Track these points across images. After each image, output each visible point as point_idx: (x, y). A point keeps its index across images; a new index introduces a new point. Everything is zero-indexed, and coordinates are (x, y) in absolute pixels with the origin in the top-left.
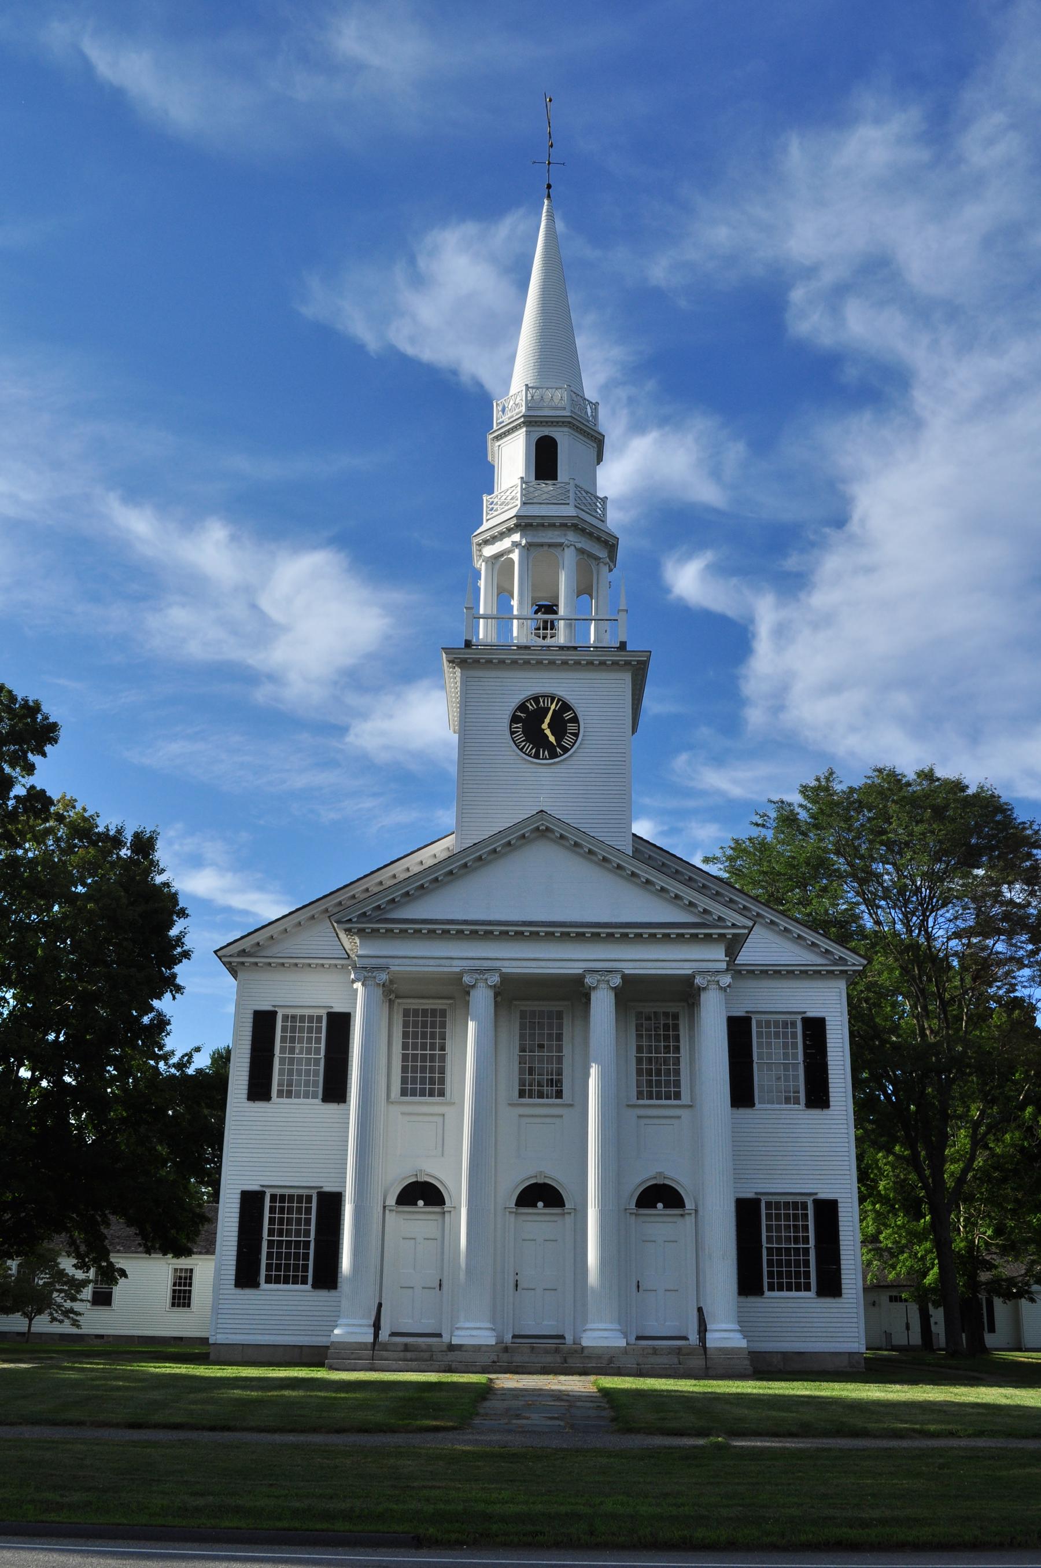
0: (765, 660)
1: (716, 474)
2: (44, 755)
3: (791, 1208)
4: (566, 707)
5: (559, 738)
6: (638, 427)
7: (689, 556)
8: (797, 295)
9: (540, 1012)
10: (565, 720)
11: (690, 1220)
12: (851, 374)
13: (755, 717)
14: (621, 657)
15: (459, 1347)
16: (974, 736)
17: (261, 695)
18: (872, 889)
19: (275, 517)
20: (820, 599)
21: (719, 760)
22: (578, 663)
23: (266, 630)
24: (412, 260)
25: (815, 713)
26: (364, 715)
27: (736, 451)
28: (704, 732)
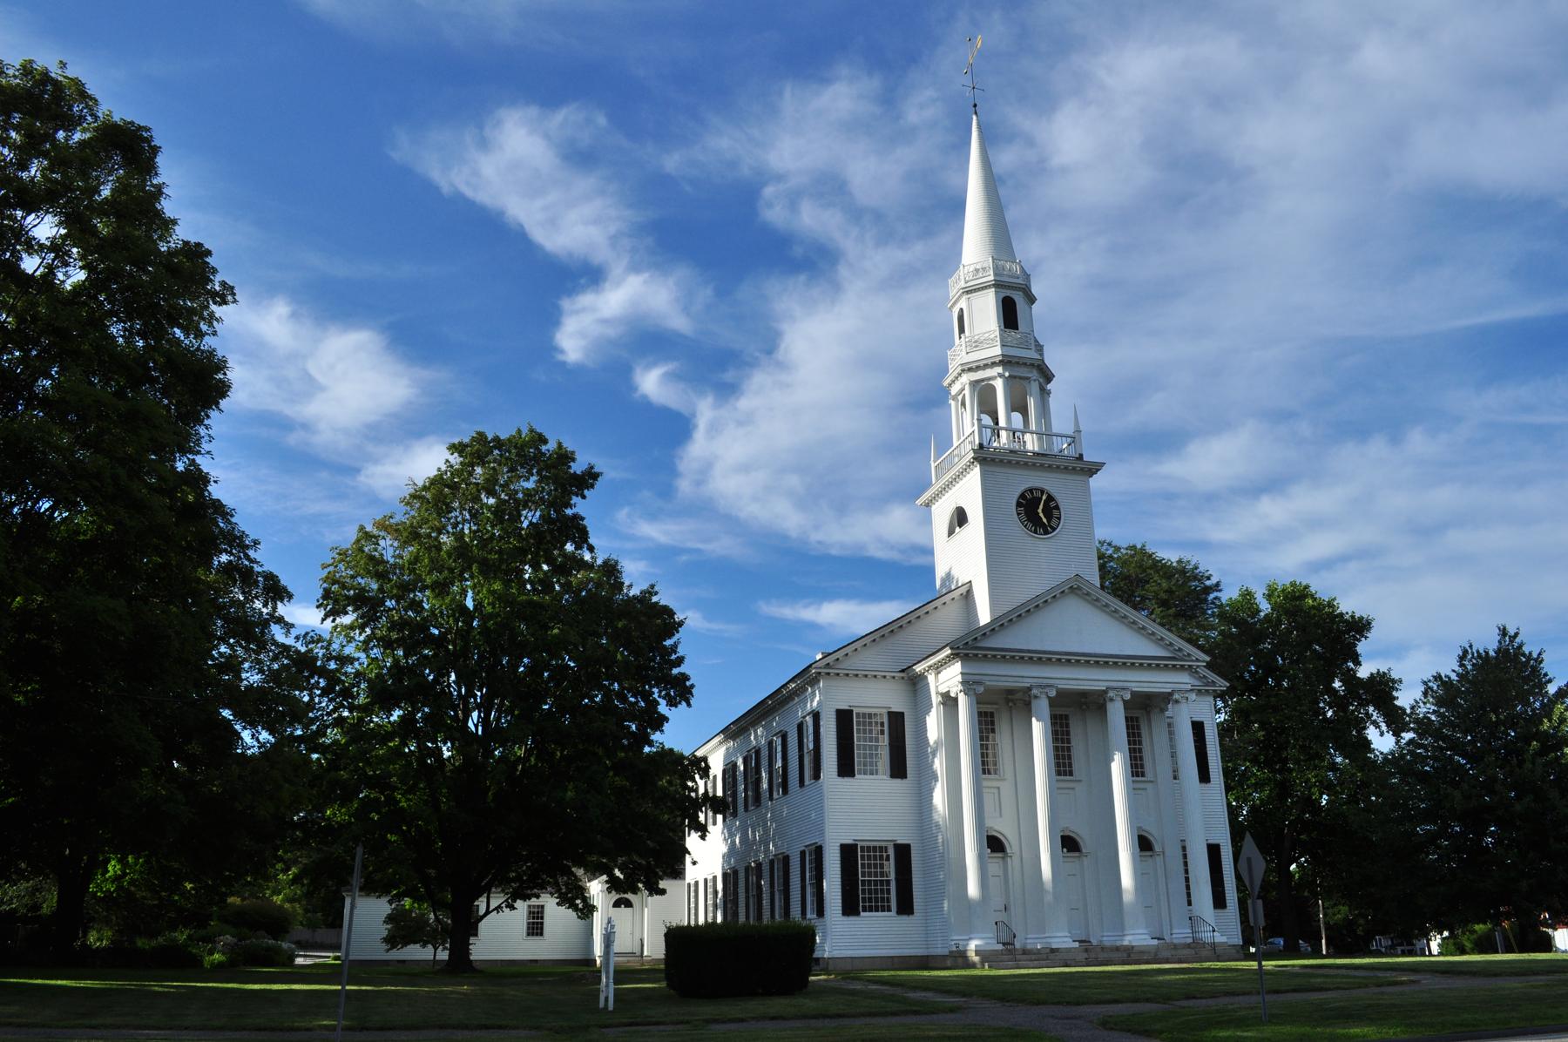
0: (699, 447)
1: (686, 310)
2: (584, 497)
3: (877, 851)
4: (1050, 498)
5: (1049, 518)
6: (635, 268)
7: (654, 364)
8: (769, 191)
9: (1074, 713)
10: (1052, 508)
11: (1159, 859)
12: (798, 251)
13: (684, 486)
14: (1079, 465)
15: (1057, 950)
16: (842, 508)
17: (293, 439)
18: (1214, 634)
19: (333, 303)
20: (744, 403)
21: (653, 516)
22: (1050, 466)
23: (311, 387)
24: (481, 127)
25: (729, 486)
26: (376, 461)
27: (706, 294)
28: (646, 494)
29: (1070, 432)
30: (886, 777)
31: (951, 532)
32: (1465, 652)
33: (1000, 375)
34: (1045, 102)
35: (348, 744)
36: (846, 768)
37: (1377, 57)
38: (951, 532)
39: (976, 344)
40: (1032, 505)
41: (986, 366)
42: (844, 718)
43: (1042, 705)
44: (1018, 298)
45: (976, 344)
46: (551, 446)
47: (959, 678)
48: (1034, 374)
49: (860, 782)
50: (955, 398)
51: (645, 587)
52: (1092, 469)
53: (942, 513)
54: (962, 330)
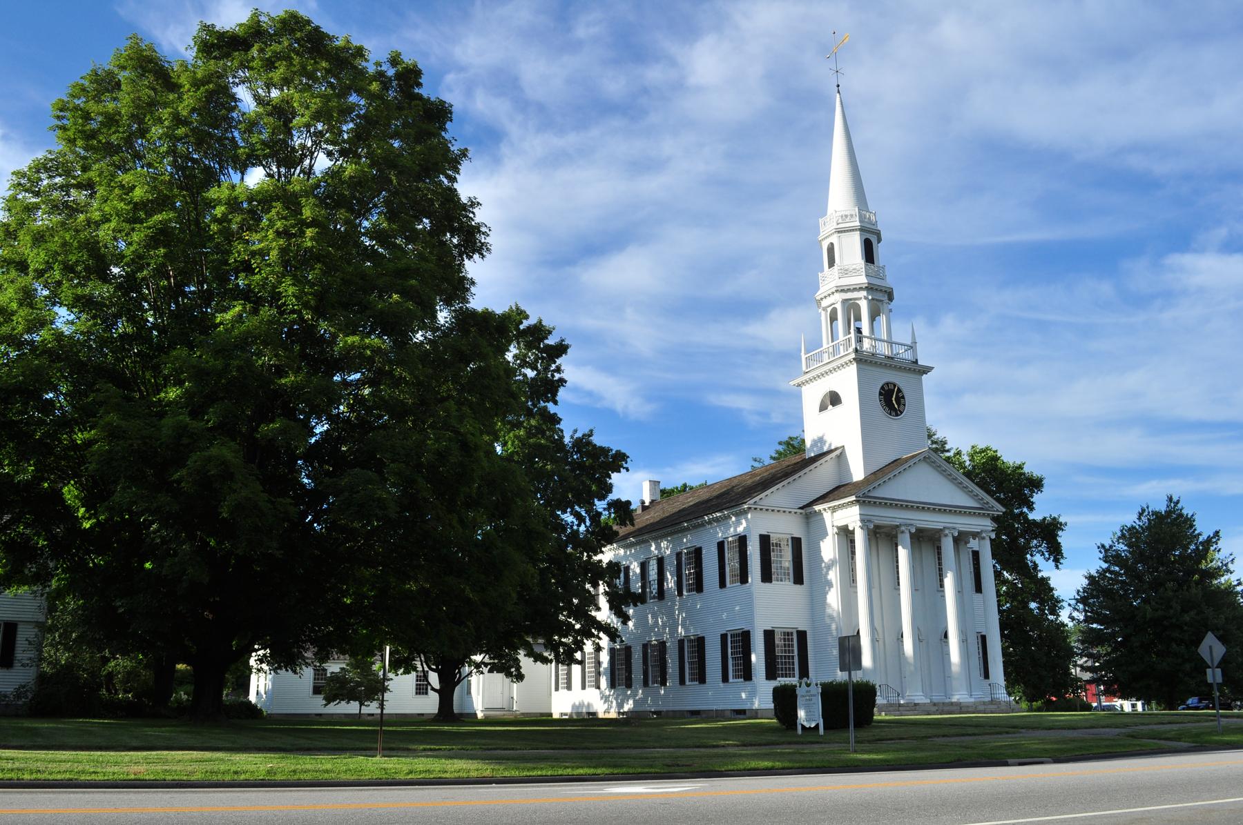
4: (899, 390)
8: (450, 78)
14: (913, 367)
29: (909, 342)
30: (791, 583)
31: (823, 408)
32: (1143, 510)
33: (866, 298)
34: (689, 31)
35: (589, 557)
36: (767, 577)
37: (951, 31)
38: (823, 408)
39: (845, 272)
40: (890, 397)
41: (855, 290)
42: (765, 540)
43: (906, 538)
44: (874, 239)
45: (845, 272)
46: (532, 321)
47: (858, 517)
48: (885, 298)
49: (775, 586)
50: (825, 309)
51: (587, 432)
52: (926, 370)
53: (812, 395)
54: (832, 263)
